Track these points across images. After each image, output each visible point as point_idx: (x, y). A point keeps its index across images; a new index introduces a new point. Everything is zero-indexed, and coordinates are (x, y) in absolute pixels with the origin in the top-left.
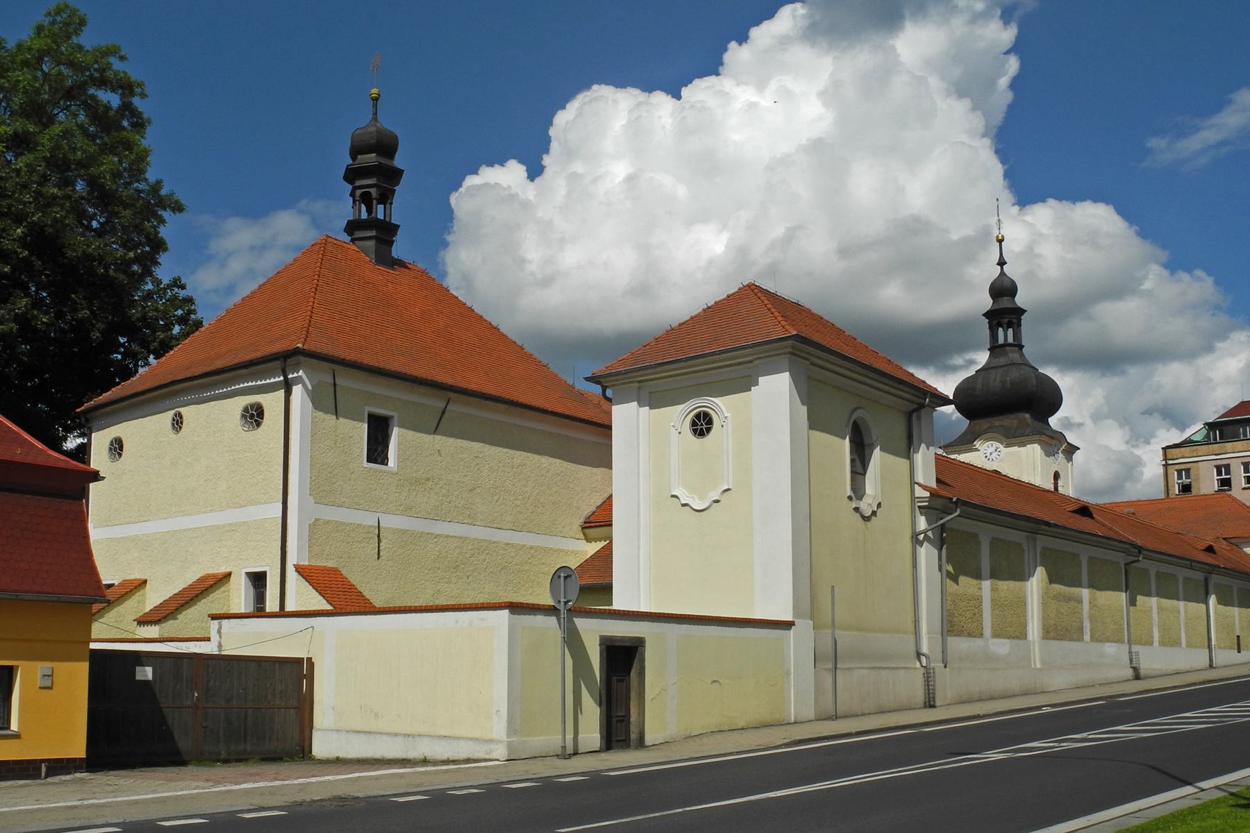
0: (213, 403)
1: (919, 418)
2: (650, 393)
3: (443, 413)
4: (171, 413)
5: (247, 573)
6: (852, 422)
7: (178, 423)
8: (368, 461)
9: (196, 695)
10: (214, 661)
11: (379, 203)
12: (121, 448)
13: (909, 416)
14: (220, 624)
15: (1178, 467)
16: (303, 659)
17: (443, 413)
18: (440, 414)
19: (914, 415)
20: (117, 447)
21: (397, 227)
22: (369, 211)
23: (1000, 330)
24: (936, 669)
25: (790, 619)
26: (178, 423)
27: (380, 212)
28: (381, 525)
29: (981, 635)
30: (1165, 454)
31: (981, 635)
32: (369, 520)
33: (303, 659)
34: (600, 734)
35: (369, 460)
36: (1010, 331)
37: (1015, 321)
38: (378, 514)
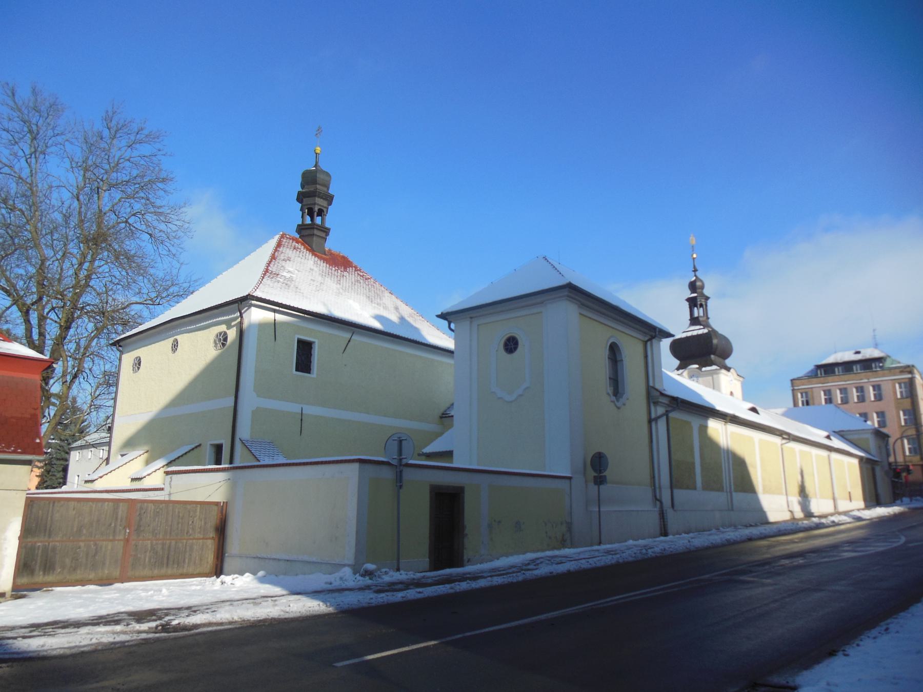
0: (196, 333)
1: (652, 345)
2: (478, 325)
3: (349, 341)
4: (171, 340)
5: (211, 445)
6: (609, 345)
7: (175, 346)
8: (296, 371)
9: (128, 531)
10: (145, 504)
11: (318, 216)
12: (140, 364)
13: (645, 343)
14: (171, 478)
15: (801, 391)
16: (26, 497)
17: (349, 341)
18: (347, 342)
19: (649, 343)
20: (138, 363)
21: (329, 229)
22: (312, 219)
23: (696, 308)
24: (883, 387)
25: (570, 475)
26: (175, 346)
27: (318, 220)
28: (303, 412)
29: (695, 488)
30: (793, 385)
31: (695, 488)
32: (294, 408)
33: (26, 497)
34: (429, 558)
35: (297, 370)
36: (701, 310)
37: (704, 303)
38: (301, 406)
